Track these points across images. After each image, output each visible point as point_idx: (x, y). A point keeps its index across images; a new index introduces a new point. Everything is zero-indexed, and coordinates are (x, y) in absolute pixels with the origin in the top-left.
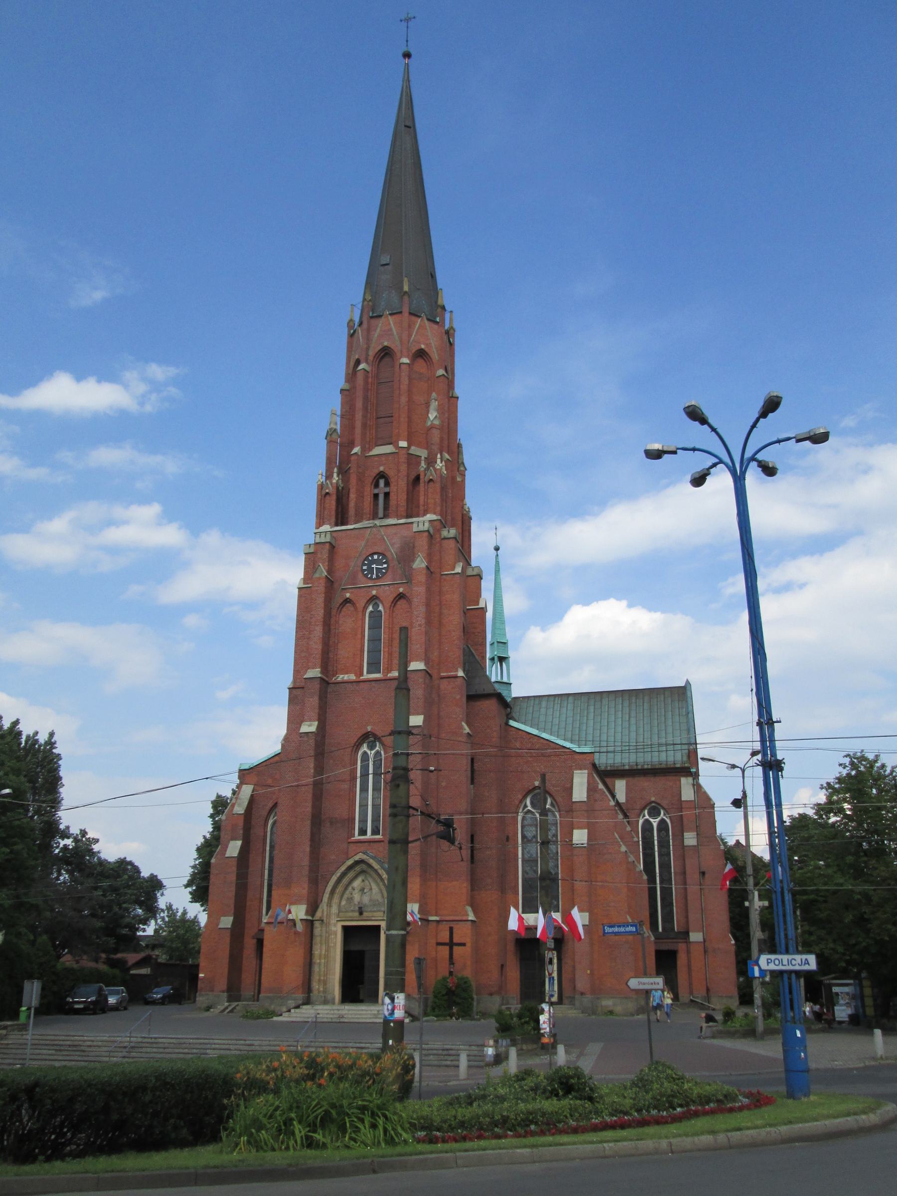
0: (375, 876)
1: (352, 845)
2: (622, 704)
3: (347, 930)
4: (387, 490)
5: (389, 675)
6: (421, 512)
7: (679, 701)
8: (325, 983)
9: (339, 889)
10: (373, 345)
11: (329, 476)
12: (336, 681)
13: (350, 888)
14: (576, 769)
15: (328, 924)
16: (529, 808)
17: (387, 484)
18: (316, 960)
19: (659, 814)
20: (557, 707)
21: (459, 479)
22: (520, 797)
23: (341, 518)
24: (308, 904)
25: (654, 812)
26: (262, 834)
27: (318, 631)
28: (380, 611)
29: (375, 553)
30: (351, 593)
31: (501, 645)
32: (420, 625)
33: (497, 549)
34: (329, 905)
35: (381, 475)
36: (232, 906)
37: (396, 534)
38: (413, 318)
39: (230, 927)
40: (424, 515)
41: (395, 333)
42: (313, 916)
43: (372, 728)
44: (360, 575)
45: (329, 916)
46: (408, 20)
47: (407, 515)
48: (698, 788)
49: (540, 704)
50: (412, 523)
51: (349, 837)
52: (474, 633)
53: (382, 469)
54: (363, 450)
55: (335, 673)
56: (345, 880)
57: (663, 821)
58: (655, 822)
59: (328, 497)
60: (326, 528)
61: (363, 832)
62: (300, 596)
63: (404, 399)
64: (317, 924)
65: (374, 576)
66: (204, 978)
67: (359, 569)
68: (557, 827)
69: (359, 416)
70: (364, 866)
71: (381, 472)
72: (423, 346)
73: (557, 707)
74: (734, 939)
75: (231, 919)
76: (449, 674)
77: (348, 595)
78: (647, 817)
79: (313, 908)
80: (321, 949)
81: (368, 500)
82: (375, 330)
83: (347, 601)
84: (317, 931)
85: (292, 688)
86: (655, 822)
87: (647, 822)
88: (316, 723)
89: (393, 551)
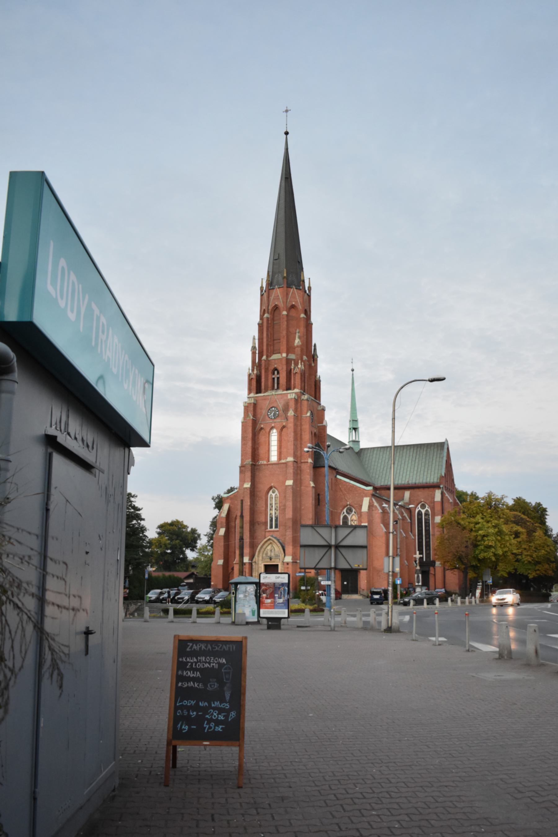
4: (278, 376)
6: (292, 388)
9: (262, 550)
10: (270, 304)
11: (253, 370)
15: (258, 564)
17: (278, 373)
19: (425, 507)
20: (381, 453)
21: (313, 365)
22: (341, 509)
23: (259, 391)
24: (249, 556)
25: (423, 506)
26: (234, 525)
27: (250, 444)
30: (264, 425)
31: (355, 422)
33: (353, 370)
34: (258, 556)
36: (223, 556)
38: (289, 289)
40: (294, 389)
41: (280, 298)
42: (252, 560)
45: (258, 560)
46: (287, 111)
47: (286, 388)
49: (373, 452)
51: (265, 530)
53: (276, 366)
54: (267, 357)
55: (258, 461)
56: (264, 547)
57: (427, 510)
58: (423, 511)
60: (252, 395)
61: (271, 527)
62: (243, 426)
63: (284, 333)
66: (213, 585)
67: (266, 414)
69: (265, 340)
70: (271, 541)
72: (294, 303)
73: (381, 453)
78: (420, 509)
79: (252, 557)
80: (255, 574)
81: (270, 381)
82: (272, 296)
84: (254, 567)
86: (423, 511)
87: (419, 511)
89: (281, 406)
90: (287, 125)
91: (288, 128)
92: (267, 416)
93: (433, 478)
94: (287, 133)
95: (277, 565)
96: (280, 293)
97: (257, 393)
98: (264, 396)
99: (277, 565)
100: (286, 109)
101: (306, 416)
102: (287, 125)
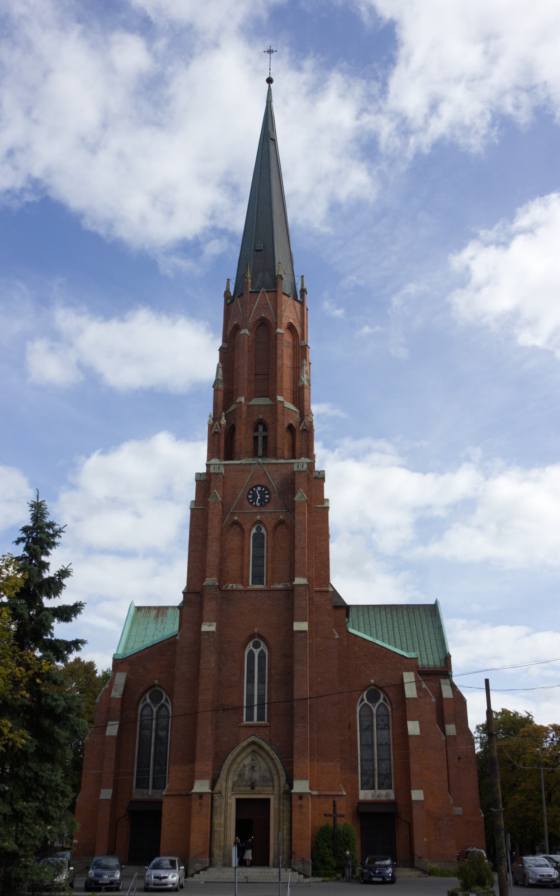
0: (264, 755)
2: (386, 616)
3: (238, 801)
4: (265, 434)
7: (431, 616)
12: (226, 589)
14: (405, 671)
16: (366, 701)
18: (216, 828)
28: (263, 534)
29: (259, 486)
35: (261, 422)
39: (110, 798)
40: (299, 458)
43: (258, 630)
44: (246, 502)
48: (453, 687)
50: (293, 463)
53: (261, 416)
56: (239, 760)
61: (250, 717)
67: (245, 497)
68: (388, 718)
71: (261, 419)
74: (484, 814)
75: (110, 791)
76: (322, 588)
77: (236, 518)
85: (187, 593)
88: (215, 624)
89: (274, 485)
90: (270, 69)
91: (271, 74)
94: (270, 81)
95: (268, 800)
96: (270, 299)
97: (226, 459)
98: (241, 464)
99: (268, 800)
100: (269, 49)
101: (323, 506)
102: (270, 69)
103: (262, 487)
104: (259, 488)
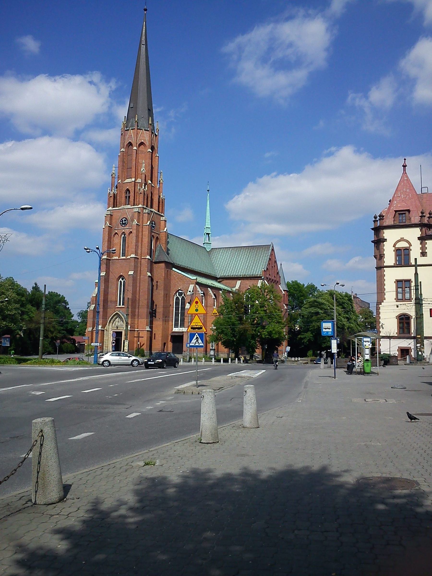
1: (116, 309)
5: (127, 257)
8: (107, 347)
13: (115, 321)
15: (108, 331)
32: (134, 243)
37: (130, 211)
40: (138, 205)
52: (162, 240)
53: (128, 187)
59: (111, 197)
64: (105, 331)
65: (127, 222)
72: (143, 141)
77: (116, 231)
79: (104, 326)
81: (124, 199)
83: (116, 233)
92: (120, 224)
93: (258, 271)
103: (125, 218)
104: (124, 219)
